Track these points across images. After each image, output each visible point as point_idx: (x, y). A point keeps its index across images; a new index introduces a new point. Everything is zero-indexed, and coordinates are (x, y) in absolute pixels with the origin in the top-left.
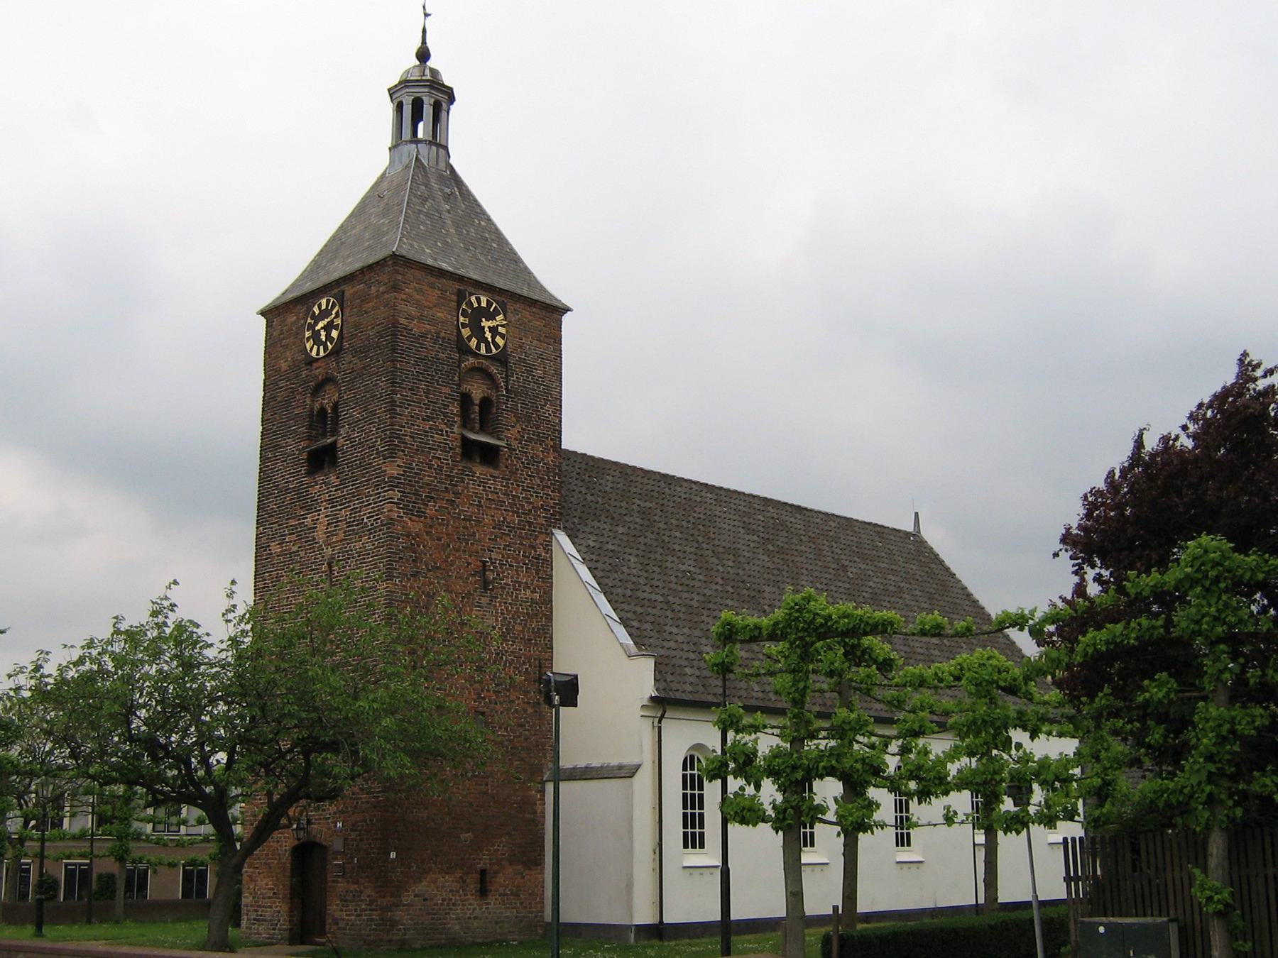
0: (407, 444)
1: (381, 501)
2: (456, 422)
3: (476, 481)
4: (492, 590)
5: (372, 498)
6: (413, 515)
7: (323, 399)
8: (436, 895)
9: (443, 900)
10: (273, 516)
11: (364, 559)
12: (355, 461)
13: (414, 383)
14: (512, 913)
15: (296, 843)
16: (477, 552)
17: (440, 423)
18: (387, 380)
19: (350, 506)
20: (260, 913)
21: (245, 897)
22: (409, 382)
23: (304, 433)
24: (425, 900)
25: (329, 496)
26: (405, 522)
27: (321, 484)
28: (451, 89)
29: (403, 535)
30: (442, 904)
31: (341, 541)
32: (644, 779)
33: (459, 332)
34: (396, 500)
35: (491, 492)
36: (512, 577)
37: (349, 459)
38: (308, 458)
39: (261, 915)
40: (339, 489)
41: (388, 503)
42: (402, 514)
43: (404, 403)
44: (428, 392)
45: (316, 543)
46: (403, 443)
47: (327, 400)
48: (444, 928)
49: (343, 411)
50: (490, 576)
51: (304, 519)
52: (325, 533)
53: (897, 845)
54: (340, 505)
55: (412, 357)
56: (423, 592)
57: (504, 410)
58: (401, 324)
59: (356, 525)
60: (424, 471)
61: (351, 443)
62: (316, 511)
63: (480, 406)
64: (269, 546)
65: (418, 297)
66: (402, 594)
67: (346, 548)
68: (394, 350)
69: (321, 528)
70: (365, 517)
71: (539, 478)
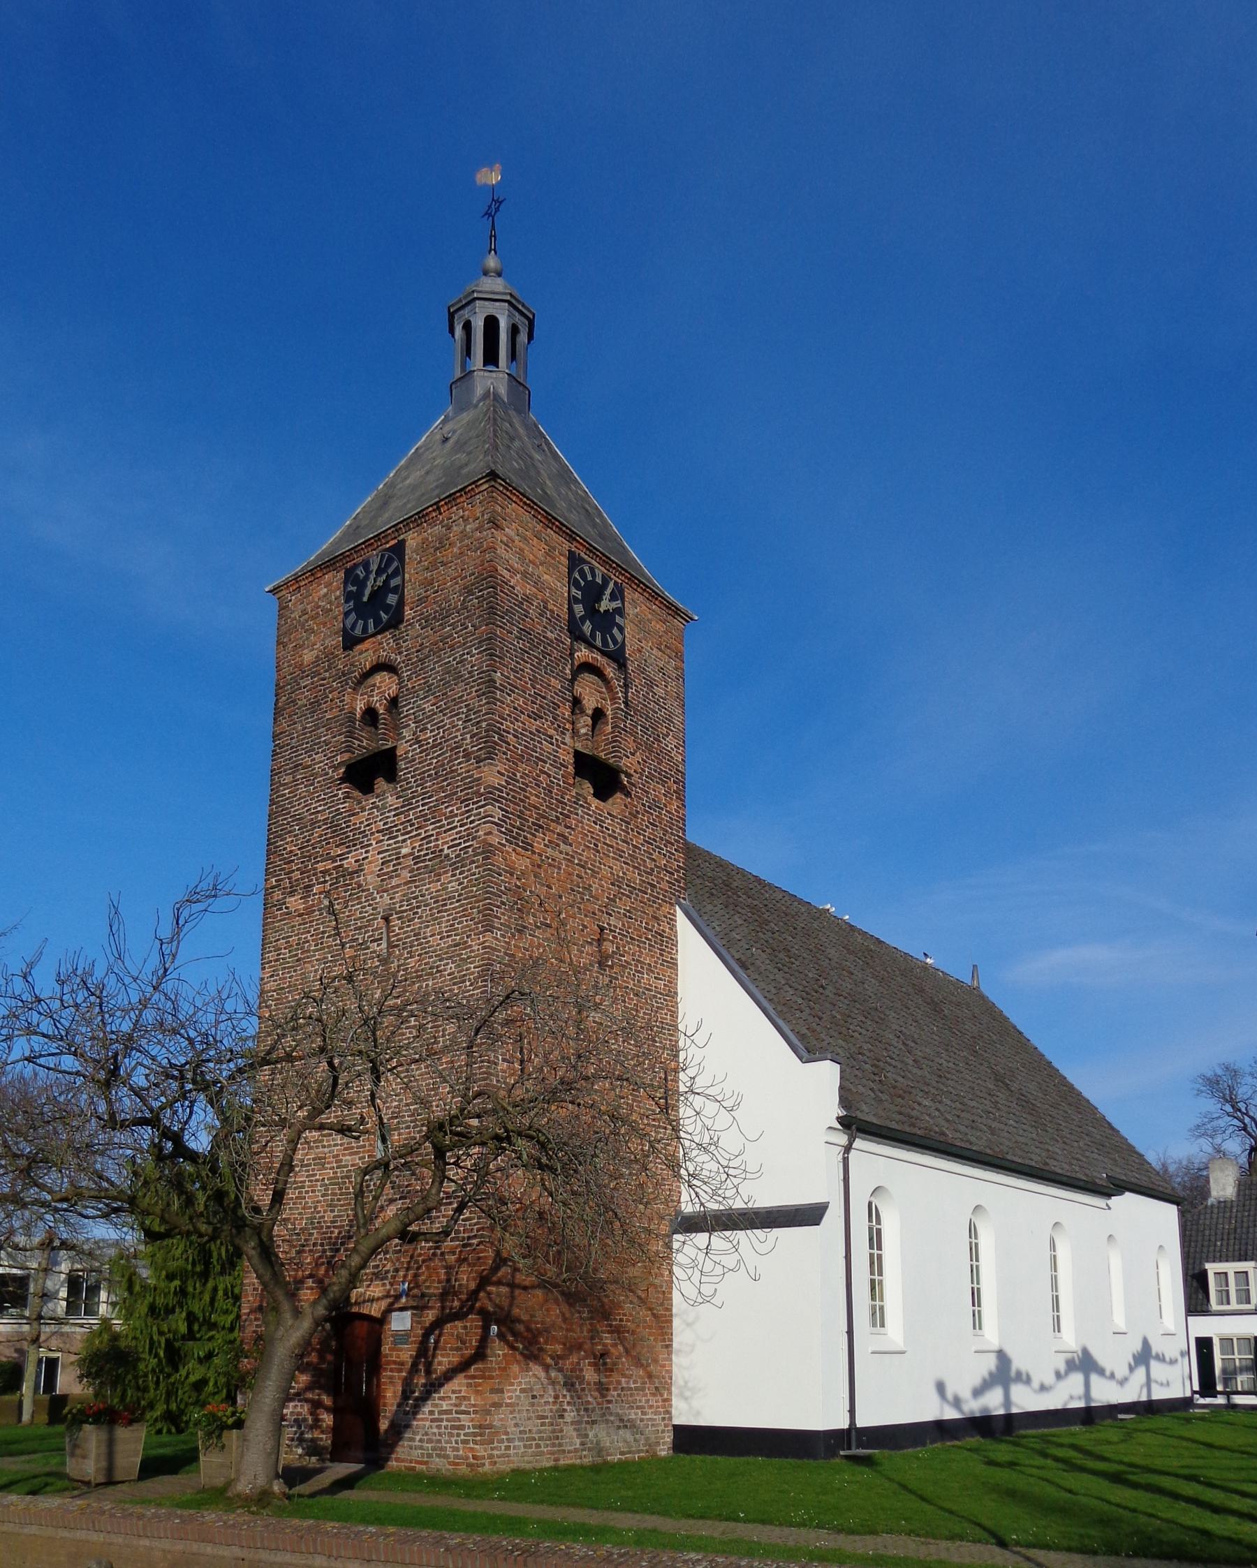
1: (472, 822)
4: (611, 967)
5: (457, 819)
7: (372, 696)
11: (445, 905)
12: (430, 770)
13: (517, 662)
16: (594, 913)
19: (419, 834)
23: (342, 743)
26: (508, 852)
27: (372, 808)
31: (406, 884)
32: (834, 1217)
34: (496, 820)
35: (609, 835)
36: (633, 954)
41: (484, 823)
42: (504, 842)
44: (534, 680)
49: (405, 706)
52: (378, 876)
53: (974, 1328)
54: (402, 835)
58: (501, 575)
59: (430, 860)
60: (531, 787)
62: (362, 848)
66: (506, 954)
67: (414, 892)
68: (492, 610)
70: (446, 847)
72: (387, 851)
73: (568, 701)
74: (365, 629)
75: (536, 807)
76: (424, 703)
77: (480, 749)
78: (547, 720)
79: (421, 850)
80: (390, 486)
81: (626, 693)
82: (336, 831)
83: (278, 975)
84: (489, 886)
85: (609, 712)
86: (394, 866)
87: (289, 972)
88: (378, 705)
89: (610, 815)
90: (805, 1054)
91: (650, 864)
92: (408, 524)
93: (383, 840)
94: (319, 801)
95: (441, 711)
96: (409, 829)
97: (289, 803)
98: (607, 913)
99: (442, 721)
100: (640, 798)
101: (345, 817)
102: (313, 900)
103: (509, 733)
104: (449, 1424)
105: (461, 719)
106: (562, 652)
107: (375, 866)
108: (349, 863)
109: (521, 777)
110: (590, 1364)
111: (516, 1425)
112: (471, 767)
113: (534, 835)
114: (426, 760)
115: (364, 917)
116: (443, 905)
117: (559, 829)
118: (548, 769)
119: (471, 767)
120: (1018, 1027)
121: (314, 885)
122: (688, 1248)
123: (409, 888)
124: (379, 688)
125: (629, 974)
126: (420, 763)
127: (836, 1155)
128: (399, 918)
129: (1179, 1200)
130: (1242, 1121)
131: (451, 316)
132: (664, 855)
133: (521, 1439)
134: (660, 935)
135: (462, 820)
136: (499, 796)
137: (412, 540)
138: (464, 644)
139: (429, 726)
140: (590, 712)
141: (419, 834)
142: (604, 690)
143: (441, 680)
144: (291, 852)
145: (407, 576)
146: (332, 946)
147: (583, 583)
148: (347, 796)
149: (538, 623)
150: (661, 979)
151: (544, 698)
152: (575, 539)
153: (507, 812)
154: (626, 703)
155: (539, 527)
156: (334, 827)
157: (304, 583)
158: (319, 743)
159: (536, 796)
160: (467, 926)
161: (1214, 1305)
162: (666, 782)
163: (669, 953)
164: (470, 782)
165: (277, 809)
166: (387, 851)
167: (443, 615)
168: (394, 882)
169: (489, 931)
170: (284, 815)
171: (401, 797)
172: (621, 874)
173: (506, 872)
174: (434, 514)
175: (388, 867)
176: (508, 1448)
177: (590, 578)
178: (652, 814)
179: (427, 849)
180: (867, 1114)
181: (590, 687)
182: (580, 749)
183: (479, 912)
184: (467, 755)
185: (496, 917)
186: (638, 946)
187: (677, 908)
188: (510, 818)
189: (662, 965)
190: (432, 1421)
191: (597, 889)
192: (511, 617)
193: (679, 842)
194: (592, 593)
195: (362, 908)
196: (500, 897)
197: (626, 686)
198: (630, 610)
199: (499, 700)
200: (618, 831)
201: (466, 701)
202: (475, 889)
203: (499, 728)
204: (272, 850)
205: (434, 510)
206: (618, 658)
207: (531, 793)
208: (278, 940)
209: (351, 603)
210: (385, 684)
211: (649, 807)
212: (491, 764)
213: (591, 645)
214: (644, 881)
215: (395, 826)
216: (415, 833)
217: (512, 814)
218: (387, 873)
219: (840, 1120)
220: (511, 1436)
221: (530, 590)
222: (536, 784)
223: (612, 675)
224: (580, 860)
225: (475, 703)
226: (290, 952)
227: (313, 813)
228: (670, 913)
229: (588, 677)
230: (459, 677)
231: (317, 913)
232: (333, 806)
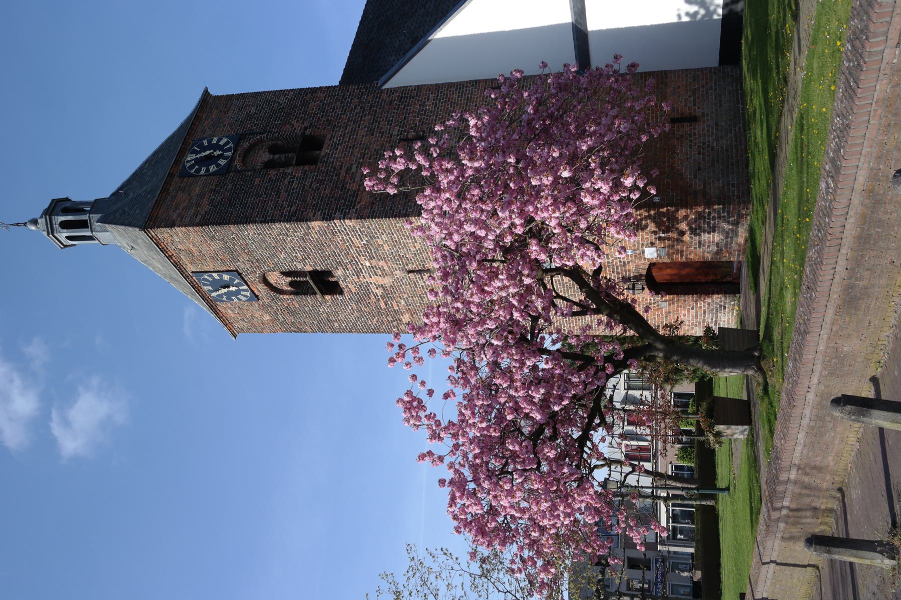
0: (297, 209)
2: (284, 171)
3: (333, 152)
4: (424, 132)
5: (345, 238)
6: (356, 200)
9: (699, 154)
10: (382, 320)
15: (647, 290)
17: (283, 184)
18: (246, 230)
20: (710, 320)
21: (696, 333)
22: (247, 211)
24: (699, 169)
25: (354, 275)
27: (346, 282)
28: (53, 200)
29: (372, 208)
31: (387, 263)
33: (214, 174)
36: (415, 117)
37: (319, 259)
38: (330, 294)
40: (346, 266)
42: (354, 210)
43: (264, 215)
46: (296, 213)
47: (284, 283)
48: (727, 150)
49: (285, 268)
50: (412, 134)
51: (378, 296)
55: (227, 210)
57: (279, 134)
58: (200, 220)
60: (320, 194)
62: (369, 286)
63: (274, 154)
65: (181, 209)
69: (380, 280)
70: (362, 243)
71: (336, 103)
72: (369, 274)
73: (267, 172)
75: (332, 190)
77: (302, 227)
81: (257, 133)
86: (377, 269)
97: (350, 323)
98: (391, 137)
100: (319, 119)
105: (286, 238)
108: (379, 292)
114: (313, 255)
115: (409, 283)
117: (343, 173)
118: (308, 183)
125: (427, 119)
128: (407, 265)
131: (65, 246)
132: (352, 99)
136: (328, 215)
141: (357, 256)
147: (197, 167)
150: (429, 97)
153: (336, 209)
162: (307, 101)
163: (411, 92)
166: (369, 274)
167: (231, 252)
168: (386, 268)
170: (356, 325)
171: (337, 268)
172: (366, 129)
175: (378, 272)
176: (733, 185)
178: (328, 110)
179: (365, 253)
186: (409, 114)
187: (383, 88)
188: (340, 208)
189: (419, 97)
191: (377, 145)
192: (223, 213)
193: (343, 90)
196: (387, 210)
202: (384, 226)
205: (172, 258)
209: (233, 298)
211: (323, 113)
215: (354, 269)
216: (356, 259)
217: (337, 206)
221: (205, 201)
222: (318, 191)
227: (353, 311)
228: (387, 93)
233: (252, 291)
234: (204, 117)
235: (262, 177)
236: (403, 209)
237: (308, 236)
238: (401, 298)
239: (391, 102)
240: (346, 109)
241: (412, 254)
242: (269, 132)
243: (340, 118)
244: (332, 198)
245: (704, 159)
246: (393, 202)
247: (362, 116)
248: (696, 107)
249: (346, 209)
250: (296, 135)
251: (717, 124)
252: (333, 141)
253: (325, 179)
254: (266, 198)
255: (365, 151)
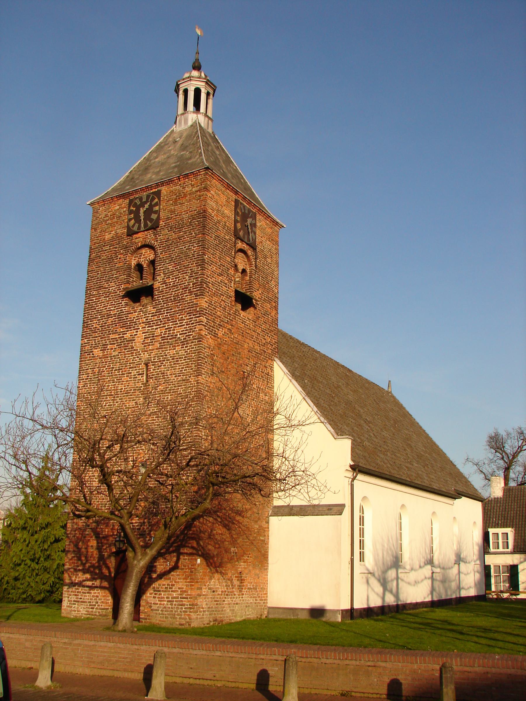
5: (184, 321)
7: (140, 258)
8: (218, 588)
11: (178, 361)
12: (171, 297)
14: (253, 600)
19: (165, 326)
23: (125, 279)
26: (208, 338)
27: (140, 311)
30: (222, 594)
31: (157, 349)
32: (347, 511)
35: (248, 328)
36: (256, 384)
39: (81, 598)
42: (207, 334)
45: (134, 350)
49: (159, 266)
53: (361, 561)
54: (155, 326)
56: (216, 387)
60: (218, 307)
61: (166, 286)
62: (134, 330)
64: (92, 352)
70: (178, 334)
73: (233, 267)
74: (139, 228)
76: (168, 266)
78: (224, 276)
79: (166, 334)
80: (147, 159)
81: (256, 262)
82: (121, 320)
83: (87, 386)
84: (201, 355)
85: (248, 271)
87: (93, 385)
88: (143, 263)
89: (249, 319)
90: (335, 436)
91: (264, 341)
92: (163, 183)
93: (145, 327)
94: (112, 305)
95: (177, 271)
96: (159, 323)
97: (95, 304)
99: (178, 275)
100: (260, 311)
101: (126, 314)
102: (107, 352)
103: (210, 283)
104: (177, 603)
106: (231, 245)
107: (141, 339)
109: (214, 303)
110: (236, 577)
111: (207, 604)
112: (193, 298)
113: (219, 330)
114: (169, 292)
116: (176, 361)
119: (193, 298)
120: (410, 413)
121: (108, 345)
122: (274, 521)
123: (159, 351)
124: (144, 255)
126: (166, 293)
127: (347, 481)
129: (483, 500)
130: (146, 203)
132: (270, 337)
133: (208, 611)
134: (267, 375)
135: (187, 322)
136: (206, 313)
137: (164, 190)
138: (190, 241)
139: (171, 276)
140: (240, 271)
142: (246, 260)
143: (177, 256)
144: (96, 327)
145: (161, 206)
146: (117, 375)
148: (127, 305)
149: (222, 232)
151: (224, 266)
152: (238, 194)
153: (208, 319)
154: (256, 268)
155: (224, 189)
156: (119, 317)
157: (107, 202)
158: (113, 277)
159: (220, 311)
160: (189, 372)
161: (492, 550)
164: (192, 305)
165: (89, 307)
169: (200, 375)
171: (155, 308)
173: (207, 347)
174: (177, 181)
175: (148, 340)
177: (243, 211)
178: (265, 318)
180: (362, 464)
181: (241, 259)
182: (238, 289)
183: (195, 366)
184: (190, 292)
185: (203, 369)
190: (168, 601)
194: (245, 216)
195: (133, 358)
196: (205, 359)
197: (256, 259)
198: (258, 224)
199: (206, 268)
200: (251, 326)
201: (191, 267)
203: (206, 281)
204: (85, 325)
205: (177, 179)
206: (253, 247)
207: (218, 310)
208: (88, 369)
209: (132, 215)
210: (147, 255)
212: (202, 298)
213: (242, 241)
214: (261, 349)
216: (162, 325)
217: (210, 320)
218: (147, 343)
219: (351, 466)
220: (205, 610)
222: (220, 306)
223: (250, 254)
224: (236, 341)
225: (195, 269)
226: (94, 375)
228: (271, 364)
229: (241, 254)
230: (187, 256)
231: (109, 358)
232: (119, 308)
233: (137, 233)
234: (267, 222)
235: (230, 263)
236: (205, 372)
237: (188, 293)
238: (119, 353)
239: (266, 367)
240: (264, 332)
241: (164, 371)
242: (255, 271)
243: (260, 327)
244: (215, 317)
245: (218, 594)
246: (209, 364)
247: (260, 344)
248: (247, 590)
249: (208, 327)
250: (252, 292)
251: (237, 604)
252: (247, 321)
253: (226, 312)
254: (218, 265)
255: (240, 345)
